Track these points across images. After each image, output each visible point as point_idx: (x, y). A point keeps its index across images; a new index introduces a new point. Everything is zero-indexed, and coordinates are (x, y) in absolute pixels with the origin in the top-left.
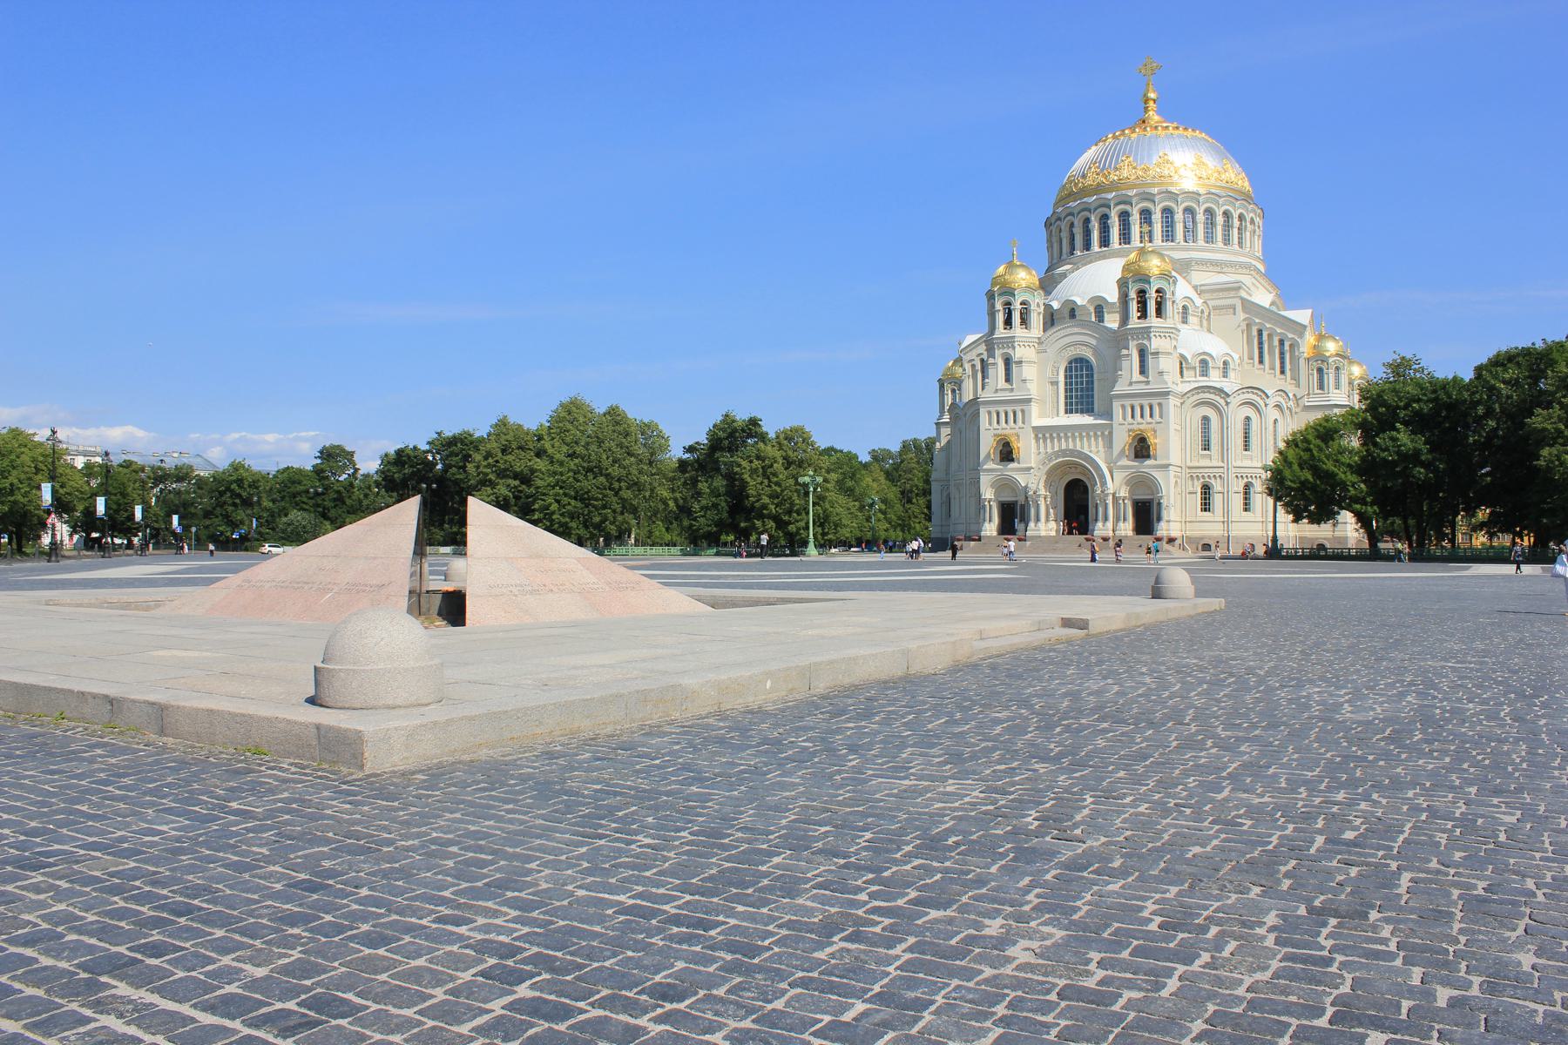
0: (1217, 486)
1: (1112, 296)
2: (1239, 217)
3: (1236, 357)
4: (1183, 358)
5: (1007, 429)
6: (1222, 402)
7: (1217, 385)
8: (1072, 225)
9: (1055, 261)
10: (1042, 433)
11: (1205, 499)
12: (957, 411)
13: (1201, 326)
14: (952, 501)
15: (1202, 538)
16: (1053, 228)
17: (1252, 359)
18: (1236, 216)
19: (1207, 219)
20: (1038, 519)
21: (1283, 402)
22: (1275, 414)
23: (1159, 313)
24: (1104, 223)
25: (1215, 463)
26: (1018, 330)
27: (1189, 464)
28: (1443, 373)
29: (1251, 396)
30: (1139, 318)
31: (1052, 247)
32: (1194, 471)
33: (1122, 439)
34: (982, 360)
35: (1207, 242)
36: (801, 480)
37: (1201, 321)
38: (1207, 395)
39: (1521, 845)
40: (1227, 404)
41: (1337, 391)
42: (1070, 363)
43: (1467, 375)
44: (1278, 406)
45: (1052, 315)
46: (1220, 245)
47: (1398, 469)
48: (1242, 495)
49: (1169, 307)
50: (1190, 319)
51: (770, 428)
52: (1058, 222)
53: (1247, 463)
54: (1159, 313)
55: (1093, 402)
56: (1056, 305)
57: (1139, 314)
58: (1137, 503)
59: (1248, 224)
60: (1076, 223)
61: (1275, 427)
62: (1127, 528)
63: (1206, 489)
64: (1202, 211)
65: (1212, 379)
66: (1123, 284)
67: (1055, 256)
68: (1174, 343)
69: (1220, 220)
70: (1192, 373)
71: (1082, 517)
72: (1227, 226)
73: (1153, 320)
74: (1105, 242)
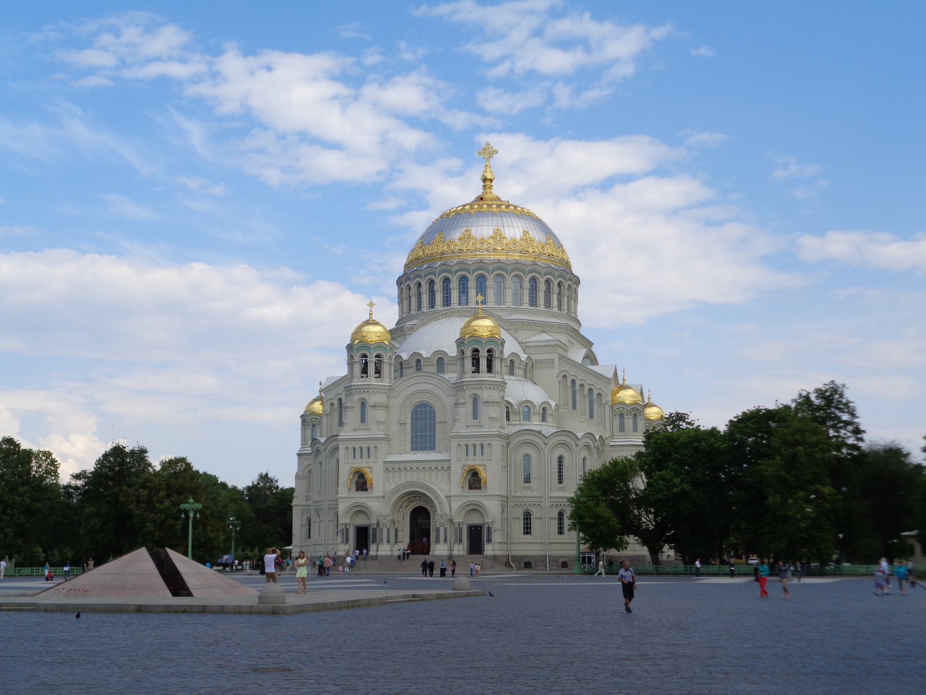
0: (535, 513)
1: (452, 351)
2: (559, 284)
3: (553, 404)
4: (509, 406)
5: (361, 463)
6: (541, 443)
7: (537, 428)
8: (419, 285)
9: (405, 315)
10: (391, 468)
11: (527, 523)
12: (317, 446)
13: (525, 377)
14: (312, 524)
15: (525, 557)
16: (404, 286)
17: (567, 405)
18: (556, 283)
19: (532, 286)
20: (437, 541)
21: (590, 441)
22: (585, 453)
23: (490, 369)
24: (447, 286)
25: (535, 494)
26: (372, 380)
27: (513, 494)
28: (705, 424)
29: (564, 438)
30: (473, 372)
31: (402, 302)
32: (517, 500)
33: (458, 473)
34: (340, 400)
35: (532, 305)
36: (182, 506)
37: (525, 373)
38: (525, 437)
39: (602, 671)
40: (577, 445)
41: (635, 434)
42: (416, 407)
43: (722, 428)
44: (587, 446)
45: (401, 364)
46: (542, 308)
47: (814, 496)
48: (556, 521)
49: (497, 364)
50: (517, 371)
51: (156, 461)
52: (408, 282)
53: (527, 493)
54: (490, 369)
55: (435, 435)
56: (405, 356)
57: (474, 368)
58: (481, 527)
59: (566, 291)
60: (423, 283)
61: (584, 463)
62: (460, 549)
63: (527, 517)
64: (528, 279)
65: (533, 423)
66: (460, 342)
67: (405, 311)
68: (502, 393)
69: (542, 287)
70: (517, 418)
71: (425, 539)
72: (548, 292)
73: (484, 376)
74: (447, 302)
